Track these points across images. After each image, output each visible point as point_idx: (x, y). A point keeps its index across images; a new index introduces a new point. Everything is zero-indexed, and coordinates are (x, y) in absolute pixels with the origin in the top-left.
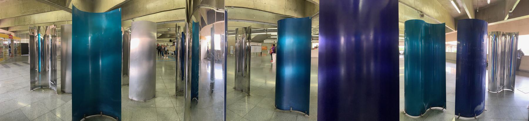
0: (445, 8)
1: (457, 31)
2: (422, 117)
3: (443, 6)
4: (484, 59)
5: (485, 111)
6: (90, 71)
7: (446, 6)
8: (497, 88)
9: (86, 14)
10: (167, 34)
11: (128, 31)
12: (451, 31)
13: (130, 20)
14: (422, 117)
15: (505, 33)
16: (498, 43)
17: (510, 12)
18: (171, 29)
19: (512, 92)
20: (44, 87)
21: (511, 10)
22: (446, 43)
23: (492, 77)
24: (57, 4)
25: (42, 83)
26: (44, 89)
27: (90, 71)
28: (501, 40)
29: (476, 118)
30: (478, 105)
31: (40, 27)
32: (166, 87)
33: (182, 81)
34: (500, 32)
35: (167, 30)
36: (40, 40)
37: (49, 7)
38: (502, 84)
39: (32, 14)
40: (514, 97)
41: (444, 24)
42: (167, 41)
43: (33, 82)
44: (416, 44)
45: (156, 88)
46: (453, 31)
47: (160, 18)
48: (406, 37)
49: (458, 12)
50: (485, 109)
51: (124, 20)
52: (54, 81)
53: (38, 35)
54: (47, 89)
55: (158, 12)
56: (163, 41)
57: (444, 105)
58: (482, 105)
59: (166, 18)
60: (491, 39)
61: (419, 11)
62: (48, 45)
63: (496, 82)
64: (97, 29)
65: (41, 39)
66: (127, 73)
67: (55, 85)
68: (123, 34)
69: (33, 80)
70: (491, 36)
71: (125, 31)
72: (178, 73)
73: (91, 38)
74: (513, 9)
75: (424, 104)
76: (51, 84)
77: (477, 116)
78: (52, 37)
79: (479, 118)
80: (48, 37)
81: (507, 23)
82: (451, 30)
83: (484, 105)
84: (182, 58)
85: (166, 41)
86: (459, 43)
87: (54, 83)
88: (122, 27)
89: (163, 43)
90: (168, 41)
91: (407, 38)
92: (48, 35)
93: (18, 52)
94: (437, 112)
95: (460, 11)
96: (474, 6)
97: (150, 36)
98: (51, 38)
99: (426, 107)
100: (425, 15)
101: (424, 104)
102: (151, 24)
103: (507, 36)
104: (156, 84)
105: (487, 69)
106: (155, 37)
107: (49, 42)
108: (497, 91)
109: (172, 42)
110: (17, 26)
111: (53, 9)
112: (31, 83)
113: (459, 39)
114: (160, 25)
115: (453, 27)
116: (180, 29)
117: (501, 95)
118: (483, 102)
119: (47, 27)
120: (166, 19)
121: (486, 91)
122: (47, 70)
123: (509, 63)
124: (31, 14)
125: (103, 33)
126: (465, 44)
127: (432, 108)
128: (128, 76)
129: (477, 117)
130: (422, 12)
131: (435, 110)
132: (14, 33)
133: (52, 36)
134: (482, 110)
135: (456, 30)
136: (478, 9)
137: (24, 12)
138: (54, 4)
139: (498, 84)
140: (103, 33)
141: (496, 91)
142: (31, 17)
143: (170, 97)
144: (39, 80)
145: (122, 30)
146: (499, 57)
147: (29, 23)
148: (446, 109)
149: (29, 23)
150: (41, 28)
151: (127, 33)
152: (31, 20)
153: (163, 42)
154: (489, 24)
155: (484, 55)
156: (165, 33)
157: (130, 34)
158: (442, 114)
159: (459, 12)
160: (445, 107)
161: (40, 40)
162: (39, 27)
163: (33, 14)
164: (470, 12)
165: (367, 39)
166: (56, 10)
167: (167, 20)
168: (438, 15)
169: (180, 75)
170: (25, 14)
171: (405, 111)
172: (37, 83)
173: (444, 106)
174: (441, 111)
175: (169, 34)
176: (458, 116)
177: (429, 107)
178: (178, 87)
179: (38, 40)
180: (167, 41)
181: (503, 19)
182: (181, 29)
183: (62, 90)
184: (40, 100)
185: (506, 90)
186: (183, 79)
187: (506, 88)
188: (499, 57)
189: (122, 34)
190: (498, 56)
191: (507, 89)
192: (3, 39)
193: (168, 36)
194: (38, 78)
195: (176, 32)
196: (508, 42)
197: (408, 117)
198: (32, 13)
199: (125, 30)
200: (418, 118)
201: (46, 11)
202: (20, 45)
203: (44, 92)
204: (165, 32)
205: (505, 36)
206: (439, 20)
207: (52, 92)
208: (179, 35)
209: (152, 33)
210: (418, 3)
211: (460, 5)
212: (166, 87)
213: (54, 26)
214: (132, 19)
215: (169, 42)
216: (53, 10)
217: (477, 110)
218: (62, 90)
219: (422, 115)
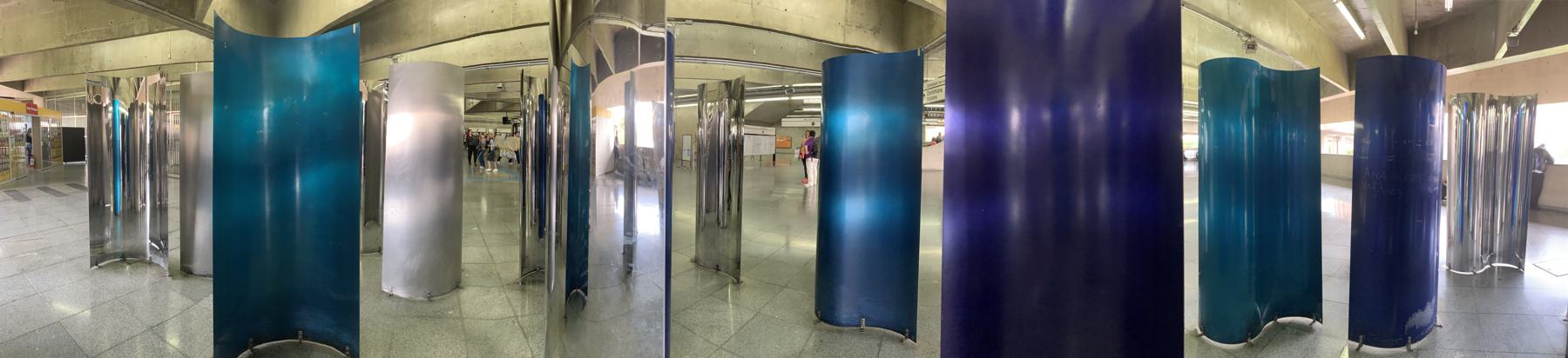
0: (1319, 23)
1: (1353, 92)
2: (1252, 345)
3: (1313, 17)
4: (1435, 175)
5: (1438, 328)
6: (268, 209)
7: (1322, 17)
8: (1472, 260)
9: (254, 41)
10: (495, 101)
11: (380, 92)
12: (1338, 91)
13: (386, 59)
15: (1497, 98)
16: (1477, 128)
17: (1512, 35)
18: (507, 85)
19: (1519, 272)
20: (131, 258)
22: (1323, 127)
23: (1459, 227)
24: (169, 12)
25: (123, 244)
26: (129, 264)
27: (268, 209)
28: (1485, 119)
29: (1410, 350)
30: (1417, 311)
31: (118, 79)
32: (491, 257)
33: (538, 241)
34: (1483, 95)
35: (495, 90)
36: (118, 118)
38: (1488, 249)
40: (1522, 288)
41: (1317, 71)
42: (494, 122)
43: (97, 244)
44: (1233, 131)
46: (1343, 92)
47: (475, 55)
48: (1202, 111)
49: (1356, 35)
50: (1439, 322)
51: (369, 58)
52: (161, 239)
53: (113, 103)
54: (140, 264)
55: (469, 37)
56: (485, 122)
57: (1315, 311)
58: (1429, 310)
59: (492, 52)
60: (1455, 115)
61: (1243, 32)
64: (289, 85)
65: (123, 115)
66: (375, 216)
67: (164, 250)
68: (364, 102)
69: (98, 237)
70: (1455, 108)
71: (370, 91)
73: (269, 114)
74: (1521, 27)
75: (1258, 309)
76: (151, 247)
77: (1413, 343)
78: (155, 108)
79: (1418, 349)
80: (143, 108)
81: (1502, 68)
85: (491, 122)
86: (1361, 126)
87: (159, 245)
88: (361, 81)
90: (499, 123)
91: (1206, 112)
92: (143, 104)
94: (1295, 331)
95: (1364, 32)
96: (1404, 17)
97: (445, 105)
98: (152, 112)
99: (1264, 316)
101: (1258, 309)
102: (449, 70)
103: (1504, 106)
104: (463, 249)
105: (1445, 205)
106: (459, 110)
107: (144, 125)
108: (1474, 268)
109: (511, 126)
110: (52, 76)
111: (157, 27)
113: (1359, 116)
114: (475, 74)
115: (1344, 79)
116: (533, 86)
117: (1486, 281)
118: (1431, 301)
119: (139, 80)
120: (492, 56)
121: (1439, 270)
122: (140, 207)
123: (1510, 187)
124: (91, 40)
125: (305, 98)
126: (1377, 132)
127: (1279, 320)
128: (379, 225)
129: (1414, 346)
131: (1290, 324)
133: (154, 106)
134: (1429, 325)
136: (1417, 26)
137: (72, 35)
139: (1477, 249)
140: (305, 98)
141: (1471, 268)
142: (91, 52)
144: (114, 236)
145: (363, 88)
146: (1480, 170)
148: (1321, 323)
149: (86, 67)
150: (123, 83)
151: (376, 99)
152: (91, 59)
153: (483, 124)
154: (1450, 72)
157: (387, 102)
158: (1310, 337)
159: (1362, 36)
161: (118, 118)
162: (116, 81)
164: (1392, 36)
165: (1089, 115)
167: (494, 58)
168: (1298, 45)
169: (533, 222)
170: (74, 41)
171: (1201, 329)
172: (109, 245)
173: (1317, 314)
174: (1308, 330)
176: (1357, 344)
177: (1271, 317)
180: (494, 122)
181: (1492, 57)
182: (535, 87)
185: (1499, 267)
187: (1499, 262)
188: (1480, 170)
189: (361, 100)
193: (499, 106)
194: (114, 231)
195: (522, 94)
196: (1506, 124)
197: (1210, 347)
198: (95, 39)
199: (370, 87)
200: (1240, 350)
201: (136, 33)
203: (131, 273)
204: (489, 94)
205: (1496, 107)
206: (1300, 60)
208: (531, 103)
210: (1240, 8)
211: (1365, 14)
212: (491, 257)
213: (162, 76)
214: (393, 55)
215: (502, 125)
216: (157, 30)
217: (1415, 326)
219: (1252, 341)
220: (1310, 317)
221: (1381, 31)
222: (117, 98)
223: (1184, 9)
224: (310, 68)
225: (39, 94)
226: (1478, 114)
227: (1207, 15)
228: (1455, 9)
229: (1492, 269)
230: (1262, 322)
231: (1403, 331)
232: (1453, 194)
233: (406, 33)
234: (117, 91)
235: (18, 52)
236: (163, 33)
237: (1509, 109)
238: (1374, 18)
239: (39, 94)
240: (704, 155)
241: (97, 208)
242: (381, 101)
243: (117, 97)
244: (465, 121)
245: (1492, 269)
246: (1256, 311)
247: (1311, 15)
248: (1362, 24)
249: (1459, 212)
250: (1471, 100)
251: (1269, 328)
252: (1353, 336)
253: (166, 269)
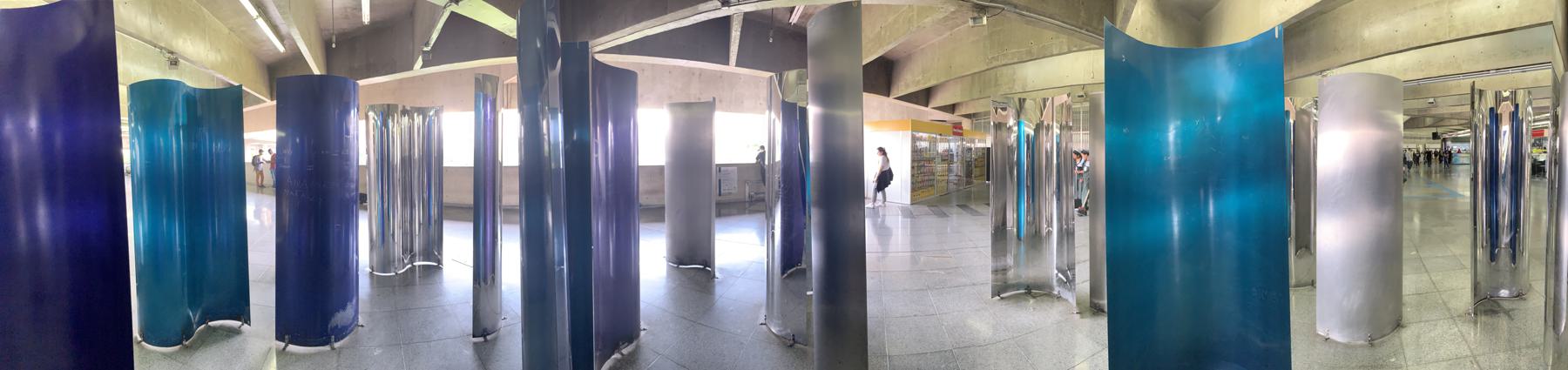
0: (239, 37)
1: (275, 102)
2: (187, 347)
3: (234, 31)
4: (352, 181)
5: (360, 328)
6: (1176, 229)
7: (242, 31)
8: (394, 261)
10: (1425, 117)
11: (1310, 110)
12: (258, 101)
13: (1314, 77)
14: (187, 347)
15: (409, 108)
16: (393, 132)
17: (425, 49)
18: (1439, 100)
19: (438, 268)
20: (1035, 291)
21: (427, 44)
22: (246, 136)
23: (380, 231)
24: (1087, 30)
25: (1029, 273)
26: (1034, 297)
27: (1176, 229)
28: (398, 126)
29: (333, 349)
30: (338, 311)
31: (1024, 100)
32: (1434, 284)
33: (1490, 264)
34: (396, 106)
35: (1425, 106)
36: (1023, 139)
37: (1064, 40)
38: (408, 250)
39: (1014, 63)
40: (441, 283)
41: (241, 86)
42: (1423, 138)
43: (999, 271)
44: (162, 144)
45: (1404, 293)
46: (264, 102)
48: (133, 125)
49: (276, 48)
50: (361, 321)
51: (1296, 76)
52: (1068, 270)
53: (1019, 124)
54: (1046, 298)
55: (1401, 51)
57: (242, 313)
58: (350, 310)
59: (1423, 67)
60: (372, 122)
61: (165, 49)
62: (1047, 152)
63: (391, 246)
64: (1202, 104)
65: (1028, 136)
66: (1306, 243)
67: (1069, 282)
68: (1292, 121)
69: (1000, 264)
70: (371, 114)
72: (1479, 235)
73: (1176, 136)
75: (191, 314)
76: (1060, 280)
77: (336, 341)
78: (1061, 128)
80: (1048, 128)
81: (422, 78)
82: (259, 99)
83: (357, 312)
84: (1491, 189)
85: (1420, 138)
86: (283, 134)
87: (1067, 277)
88: (1287, 99)
89: (1414, 143)
90: (1428, 138)
91: (136, 126)
92: (1048, 125)
93: (976, 172)
95: (284, 45)
96: (321, 30)
97: (1380, 122)
98: (1059, 132)
100: (181, 61)
101: (191, 314)
102: (1387, 82)
103: (416, 115)
104: (1404, 277)
105: (365, 208)
106: (1397, 126)
107: (1049, 143)
108: (396, 268)
109: (1440, 141)
110: (978, 99)
111: (1076, 46)
112: (995, 271)
113: (281, 124)
114: (1414, 89)
115: (265, 89)
116: (1483, 99)
117: (407, 280)
118: (351, 301)
119: (1045, 101)
120: (1423, 71)
121: (359, 273)
122: (1044, 232)
123: (426, 190)
124: (1012, 62)
125: (1219, 118)
126: (298, 140)
127: (210, 323)
128: (1311, 254)
129: (337, 345)
130: (172, 53)
131: (221, 328)
132: (969, 121)
134: (351, 324)
135: (272, 100)
136: (334, 40)
137: (993, 58)
138: (1079, 30)
139: (398, 250)
140: (1219, 118)
141: (393, 269)
142: (1014, 73)
143: (1452, 318)
144: (1017, 263)
145: (1288, 105)
147: (1009, 88)
148: (250, 325)
149: (1009, 88)
150: (1028, 104)
152: (1014, 81)
153: (1413, 140)
154: (361, 82)
155: (351, 171)
156: (1421, 114)
157: (1316, 121)
159: (282, 49)
160: (247, 320)
161: (1023, 139)
162: (1022, 101)
163: (1017, 63)
165: (22, 130)
166: (1087, 47)
167: (1424, 73)
168: (219, 59)
169: (1485, 244)
170: (995, 63)
171: (141, 336)
172: (1011, 274)
173: (245, 318)
175: (1430, 117)
176: (283, 344)
177: (203, 321)
178: (1478, 283)
179: (1019, 138)
180: (1423, 138)
181: (411, 68)
183: (1095, 304)
184: (1015, 335)
185: (419, 266)
186: (1493, 257)
187: (419, 261)
188: (398, 175)
190: (393, 169)
191: (423, 261)
192: (939, 137)
193: (1429, 121)
194: (1016, 257)
195: (1473, 107)
196: (419, 129)
198: (1016, 60)
199: (1299, 106)
200: (177, 352)
201: (1055, 53)
202: (983, 154)
203: (1034, 309)
204: (1419, 110)
205: (409, 116)
207: (1061, 308)
208: (1482, 118)
209: (1389, 113)
210: (162, 27)
211: (284, 29)
212: (1434, 284)
213: (1069, 95)
214: (1321, 72)
215: (1432, 140)
216: (1075, 49)
217: (337, 326)
218: (1096, 301)
219: (187, 343)
220: (239, 320)
221: (298, 44)
222: (1023, 120)
223: (116, 32)
224: (1224, 83)
225: (968, 116)
226: (393, 120)
227: (130, 34)
228: (372, 22)
229: (413, 268)
230: (195, 326)
231: (326, 331)
232: (374, 200)
233: (1335, 49)
234: (1023, 111)
235: (949, 79)
236: (1081, 53)
237: (421, 117)
238: (293, 34)
239: (968, 116)
240: (777, 169)
241: (1000, 232)
242: (1310, 119)
243: (1022, 117)
244: (1404, 137)
245: (415, 266)
246: (189, 317)
247: (231, 29)
248: (281, 38)
249: (380, 216)
250: (386, 109)
251: (202, 331)
252: (279, 337)
253: (1075, 305)
